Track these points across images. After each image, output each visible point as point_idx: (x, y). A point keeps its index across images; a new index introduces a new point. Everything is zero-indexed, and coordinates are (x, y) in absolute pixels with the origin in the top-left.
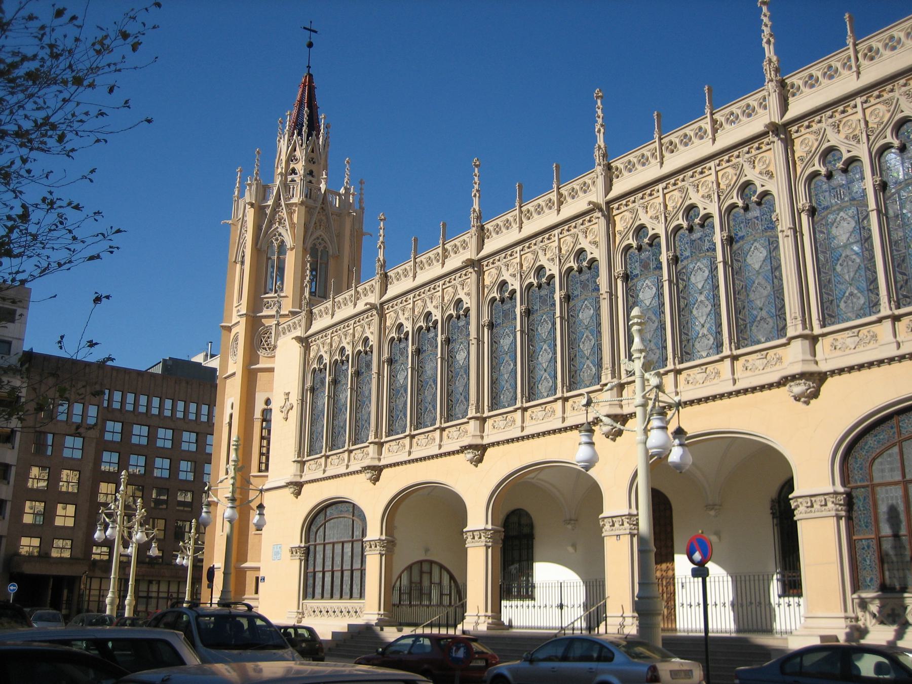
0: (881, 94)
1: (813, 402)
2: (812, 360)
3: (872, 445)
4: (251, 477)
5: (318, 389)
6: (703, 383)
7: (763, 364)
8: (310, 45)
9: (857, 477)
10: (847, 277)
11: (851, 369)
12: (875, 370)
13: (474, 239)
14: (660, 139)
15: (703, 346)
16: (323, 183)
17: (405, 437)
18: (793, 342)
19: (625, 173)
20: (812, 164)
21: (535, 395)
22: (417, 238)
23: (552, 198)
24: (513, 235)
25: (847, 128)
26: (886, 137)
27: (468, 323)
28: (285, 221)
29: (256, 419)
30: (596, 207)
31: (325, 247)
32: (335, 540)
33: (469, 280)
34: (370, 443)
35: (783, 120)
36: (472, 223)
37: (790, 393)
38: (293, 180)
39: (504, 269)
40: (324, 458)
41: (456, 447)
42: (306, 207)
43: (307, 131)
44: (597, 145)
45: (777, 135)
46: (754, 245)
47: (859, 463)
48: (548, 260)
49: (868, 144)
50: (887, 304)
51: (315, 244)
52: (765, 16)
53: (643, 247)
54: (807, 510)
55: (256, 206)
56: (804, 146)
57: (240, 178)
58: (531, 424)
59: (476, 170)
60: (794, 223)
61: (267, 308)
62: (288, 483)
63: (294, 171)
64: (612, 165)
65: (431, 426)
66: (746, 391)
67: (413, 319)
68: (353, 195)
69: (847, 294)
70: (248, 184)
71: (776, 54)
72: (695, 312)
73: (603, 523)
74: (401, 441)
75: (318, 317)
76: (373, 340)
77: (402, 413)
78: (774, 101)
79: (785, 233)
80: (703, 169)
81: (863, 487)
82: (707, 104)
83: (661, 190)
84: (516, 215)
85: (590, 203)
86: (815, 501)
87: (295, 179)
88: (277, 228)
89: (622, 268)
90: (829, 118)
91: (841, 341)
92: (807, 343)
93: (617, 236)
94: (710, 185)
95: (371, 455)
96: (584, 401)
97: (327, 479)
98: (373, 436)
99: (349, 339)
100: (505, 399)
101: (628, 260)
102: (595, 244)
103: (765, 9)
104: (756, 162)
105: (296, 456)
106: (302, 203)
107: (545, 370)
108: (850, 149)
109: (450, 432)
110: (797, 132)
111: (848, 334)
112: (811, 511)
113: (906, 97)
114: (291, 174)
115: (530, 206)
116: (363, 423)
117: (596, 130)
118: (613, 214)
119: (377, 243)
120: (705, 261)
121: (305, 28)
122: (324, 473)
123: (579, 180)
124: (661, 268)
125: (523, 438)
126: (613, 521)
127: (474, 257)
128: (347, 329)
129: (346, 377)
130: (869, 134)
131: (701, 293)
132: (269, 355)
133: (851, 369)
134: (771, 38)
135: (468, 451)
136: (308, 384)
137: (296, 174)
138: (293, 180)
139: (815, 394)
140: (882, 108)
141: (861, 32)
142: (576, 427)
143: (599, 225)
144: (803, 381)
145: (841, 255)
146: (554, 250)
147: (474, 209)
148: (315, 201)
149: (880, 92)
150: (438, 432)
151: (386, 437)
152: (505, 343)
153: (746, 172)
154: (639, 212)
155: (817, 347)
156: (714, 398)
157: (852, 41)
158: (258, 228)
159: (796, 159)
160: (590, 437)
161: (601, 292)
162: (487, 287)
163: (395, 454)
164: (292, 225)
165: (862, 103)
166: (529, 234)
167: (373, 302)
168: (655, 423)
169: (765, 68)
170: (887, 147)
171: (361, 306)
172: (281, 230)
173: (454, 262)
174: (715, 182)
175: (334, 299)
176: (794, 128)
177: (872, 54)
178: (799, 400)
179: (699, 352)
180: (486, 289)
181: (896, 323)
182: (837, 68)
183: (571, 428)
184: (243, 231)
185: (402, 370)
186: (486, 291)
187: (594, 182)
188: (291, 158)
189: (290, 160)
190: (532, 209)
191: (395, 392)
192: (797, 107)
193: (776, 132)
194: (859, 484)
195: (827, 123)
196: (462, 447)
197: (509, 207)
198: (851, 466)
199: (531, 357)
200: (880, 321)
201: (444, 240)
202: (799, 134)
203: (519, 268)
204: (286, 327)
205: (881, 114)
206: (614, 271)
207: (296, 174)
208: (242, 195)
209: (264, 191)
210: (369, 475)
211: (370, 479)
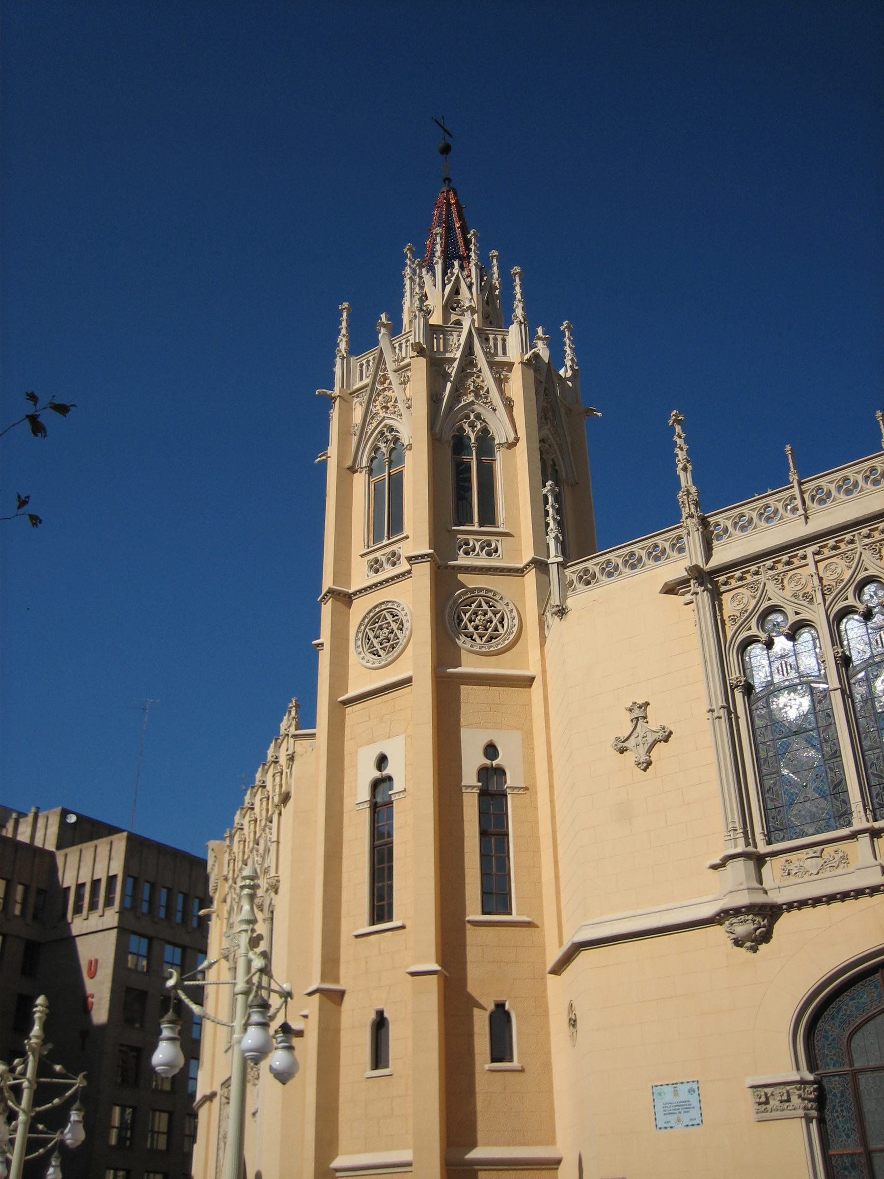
1: (763, 947)
4: (468, 926)
7: (817, 865)
12: (850, 903)
18: (730, 865)
20: (843, 597)
26: (750, 629)
29: (467, 787)
37: (730, 934)
45: (701, 584)
49: (825, 605)
50: (863, 813)
52: (680, 437)
54: (759, 1107)
56: (736, 603)
61: (467, 553)
64: (709, 519)
78: (694, 541)
79: (716, 714)
80: (728, 578)
82: (792, 469)
86: (772, 1095)
88: (472, 403)
89: (740, 673)
92: (751, 864)
103: (678, 429)
110: (725, 584)
111: (807, 854)
112: (766, 1110)
113: (775, 582)
130: (825, 592)
134: (688, 465)
139: (766, 937)
140: (840, 563)
141: (806, 471)
144: (750, 917)
154: (863, 557)
155: (763, 870)
159: (726, 617)
165: (814, 554)
168: (255, 1018)
169: (681, 500)
170: (751, 641)
176: (722, 579)
177: (823, 497)
178: (741, 946)
181: (875, 839)
182: (665, 549)
189: (449, 307)
192: (723, 554)
193: (700, 580)
200: (854, 836)
205: (839, 570)
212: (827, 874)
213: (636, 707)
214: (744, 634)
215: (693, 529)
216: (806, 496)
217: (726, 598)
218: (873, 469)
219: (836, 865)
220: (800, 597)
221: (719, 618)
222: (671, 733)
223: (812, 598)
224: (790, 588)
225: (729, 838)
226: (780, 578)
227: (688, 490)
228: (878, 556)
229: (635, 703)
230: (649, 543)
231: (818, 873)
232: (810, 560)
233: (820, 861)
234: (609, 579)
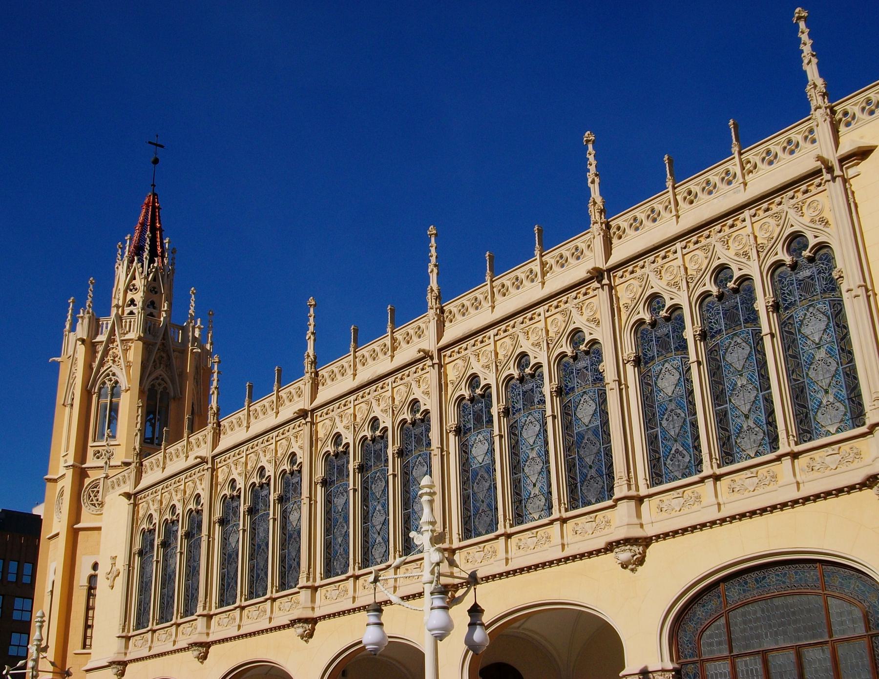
0: (809, 188)
3: (701, 617)
5: (653, 358)
6: (481, 562)
8: (156, 161)
9: (686, 653)
10: (672, 433)
11: (839, 491)
12: (698, 534)
13: (309, 386)
14: (492, 281)
15: (534, 507)
17: (497, 537)
19: (458, 317)
20: (508, 368)
21: (368, 561)
23: (533, 268)
24: (347, 383)
25: (669, 274)
26: (776, 254)
27: (428, 430)
28: (120, 358)
30: (427, 355)
31: (165, 388)
32: (766, 647)
34: (199, 616)
35: (608, 265)
36: (306, 369)
38: (131, 313)
39: (414, 385)
42: (144, 343)
46: (584, 397)
47: (688, 636)
48: (382, 411)
49: (759, 261)
50: (786, 439)
51: (153, 386)
53: (476, 398)
55: (88, 342)
57: (72, 309)
60: (619, 376)
62: (110, 663)
63: (132, 302)
64: (835, 108)
66: (574, 558)
67: (246, 475)
68: (199, 328)
69: (673, 452)
70: (82, 317)
71: (601, 194)
72: (526, 470)
75: (149, 469)
78: (824, 131)
79: (854, 293)
81: (694, 663)
83: (352, 402)
87: (134, 311)
90: (790, 198)
91: (739, 482)
93: (450, 386)
94: (540, 333)
95: (199, 629)
96: (371, 578)
97: (153, 658)
99: (180, 496)
100: (338, 565)
104: (584, 308)
105: (121, 630)
106: (140, 339)
107: (379, 534)
108: (817, 234)
114: (129, 306)
115: (365, 351)
116: (291, 563)
117: (429, 271)
119: (306, 334)
120: (536, 415)
121: (150, 143)
124: (544, 402)
125: (508, 574)
127: (308, 407)
128: (179, 484)
129: (176, 538)
130: (759, 250)
131: (819, 348)
132: (98, 513)
133: (839, 491)
135: (298, 625)
136: (137, 546)
137: (135, 305)
138: (131, 313)
139: (641, 561)
141: (680, 176)
142: (364, 608)
145: (666, 410)
146: (489, 355)
148: (154, 336)
149: (808, 186)
151: (134, 630)
153: (574, 319)
156: (544, 565)
157: (671, 184)
158: (88, 367)
159: (621, 306)
160: (379, 617)
162: (321, 440)
163: (224, 628)
164: (128, 366)
166: (396, 366)
172: (115, 369)
174: (544, 329)
179: (530, 514)
180: (319, 442)
183: (359, 609)
184: (73, 369)
185: (420, 463)
186: (450, 388)
187: (589, 246)
188: (131, 287)
191: (229, 558)
192: (621, 251)
194: (689, 659)
196: (291, 621)
200: (702, 480)
201: (356, 348)
202: (452, 359)
203: (352, 420)
204: (115, 481)
206: (446, 424)
207: (135, 305)
208: (73, 329)
209: (95, 328)
210: (196, 653)
211: (302, 637)
214: (772, 259)
215: (820, 120)
216: (495, 290)
217: (449, 368)
218: (869, 102)
219: (543, 542)
220: (817, 222)
221: (851, 201)
223: (599, 322)
224: (734, 247)
225: (874, 407)
226: (725, 240)
227: (814, 83)
228: (726, 247)
231: (754, 491)
232: (748, 222)
233: (337, 592)
234: (848, 128)
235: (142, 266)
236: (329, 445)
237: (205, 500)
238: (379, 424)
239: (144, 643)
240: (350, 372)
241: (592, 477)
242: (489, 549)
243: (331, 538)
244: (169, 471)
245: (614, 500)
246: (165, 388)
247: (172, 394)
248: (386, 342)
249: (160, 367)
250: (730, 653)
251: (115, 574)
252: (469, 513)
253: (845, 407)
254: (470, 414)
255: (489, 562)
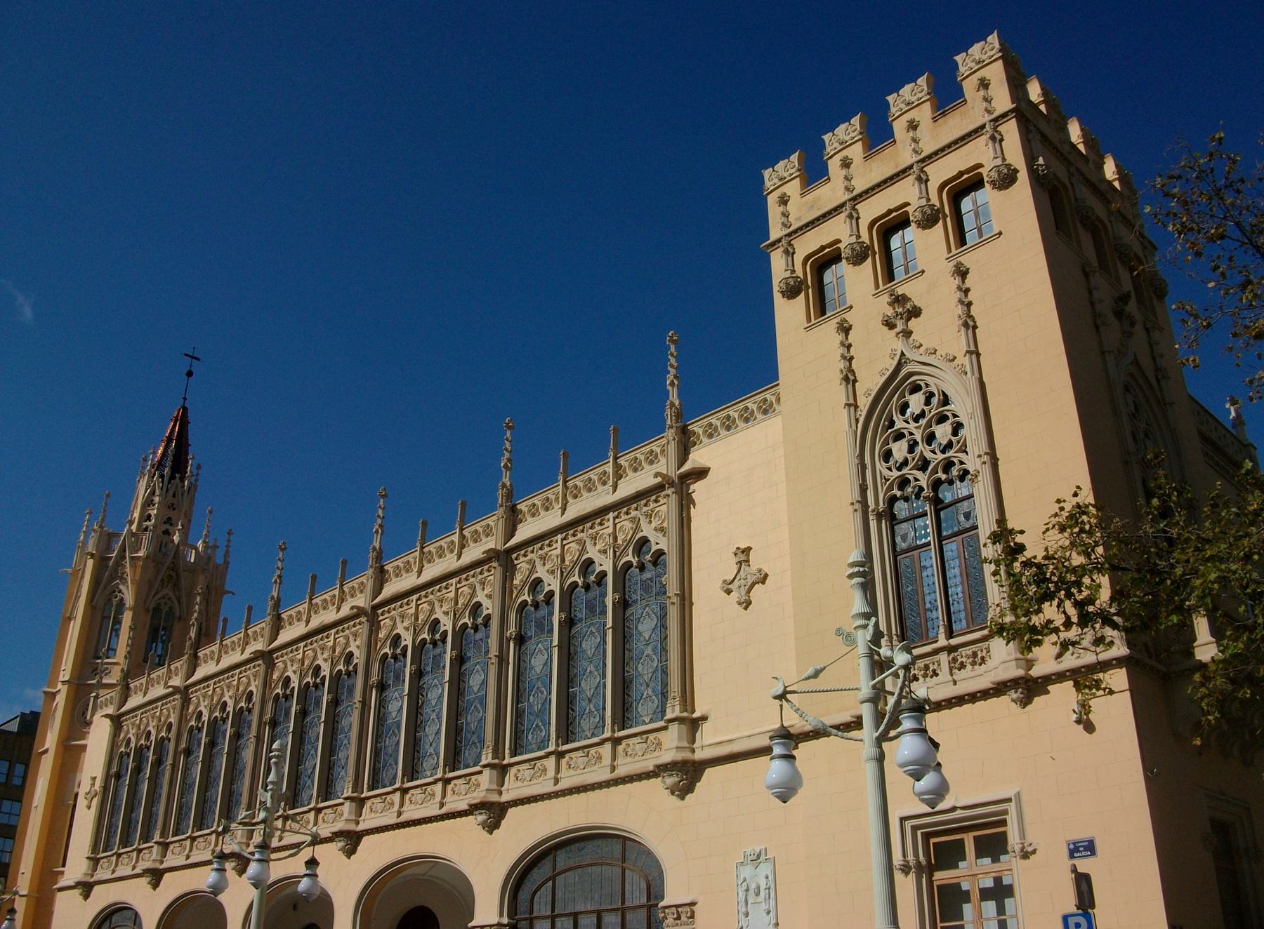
2: (687, 748)
8: (190, 374)
16: (177, 534)
22: (465, 502)
24: (553, 519)
28: (127, 576)
31: (171, 608)
32: (580, 908)
33: (492, 577)
34: (485, 766)
40: (313, 813)
41: (463, 806)
43: (169, 473)
44: (500, 484)
51: (159, 604)
58: (567, 774)
59: (508, 433)
65: (390, 786)
73: (663, 915)
74: (389, 797)
76: (359, 657)
77: (344, 770)
82: (612, 447)
83: (559, 541)
84: (334, 596)
85: (657, 475)
95: (346, 816)
98: (490, 755)
101: (573, 601)
102: (662, 531)
103: (673, 348)
109: (571, 758)
117: (668, 383)
118: (379, 619)
121: (186, 355)
122: (113, 873)
123: (483, 522)
126: (678, 912)
136: (114, 770)
143: (494, 575)
147: (191, 637)
150: (440, 785)
152: (537, 662)
154: (641, 522)
161: (668, 595)
167: (362, 605)
171: (345, 611)
172: (121, 587)
173: (473, 553)
175: (149, 675)
176: (514, 556)
179: (642, 716)
186: (515, 592)
188: (148, 503)
189: (146, 505)
190: (580, 484)
195: (588, 533)
197: (550, 481)
198: (653, 884)
199: (568, 678)
211: (342, 849)
212: (648, 756)
213: (739, 552)
222: (766, 575)
229: (738, 548)
230: (741, 406)
233: (467, 786)
235: (163, 482)
236: (426, 633)
237: (256, 699)
238: (543, 587)
239: (338, 818)
240: (558, 507)
241: (474, 743)
242: (653, 740)
243: (577, 690)
244: (149, 697)
245: (665, 720)
246: (171, 608)
247: (178, 614)
248: (454, 539)
249: (167, 586)
250: (552, 913)
251: (93, 794)
252: (523, 727)
253: (658, 700)
254: (532, 621)
255: (537, 782)
